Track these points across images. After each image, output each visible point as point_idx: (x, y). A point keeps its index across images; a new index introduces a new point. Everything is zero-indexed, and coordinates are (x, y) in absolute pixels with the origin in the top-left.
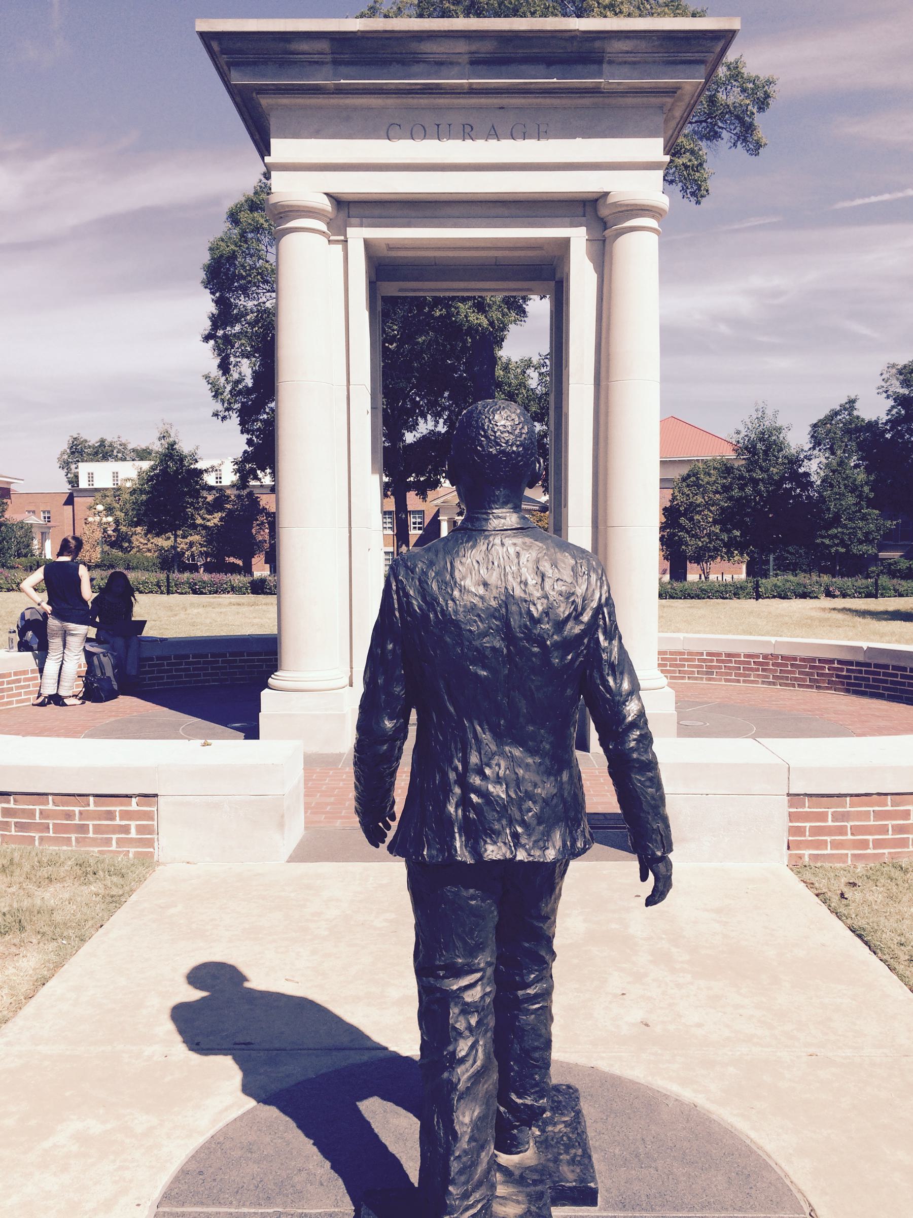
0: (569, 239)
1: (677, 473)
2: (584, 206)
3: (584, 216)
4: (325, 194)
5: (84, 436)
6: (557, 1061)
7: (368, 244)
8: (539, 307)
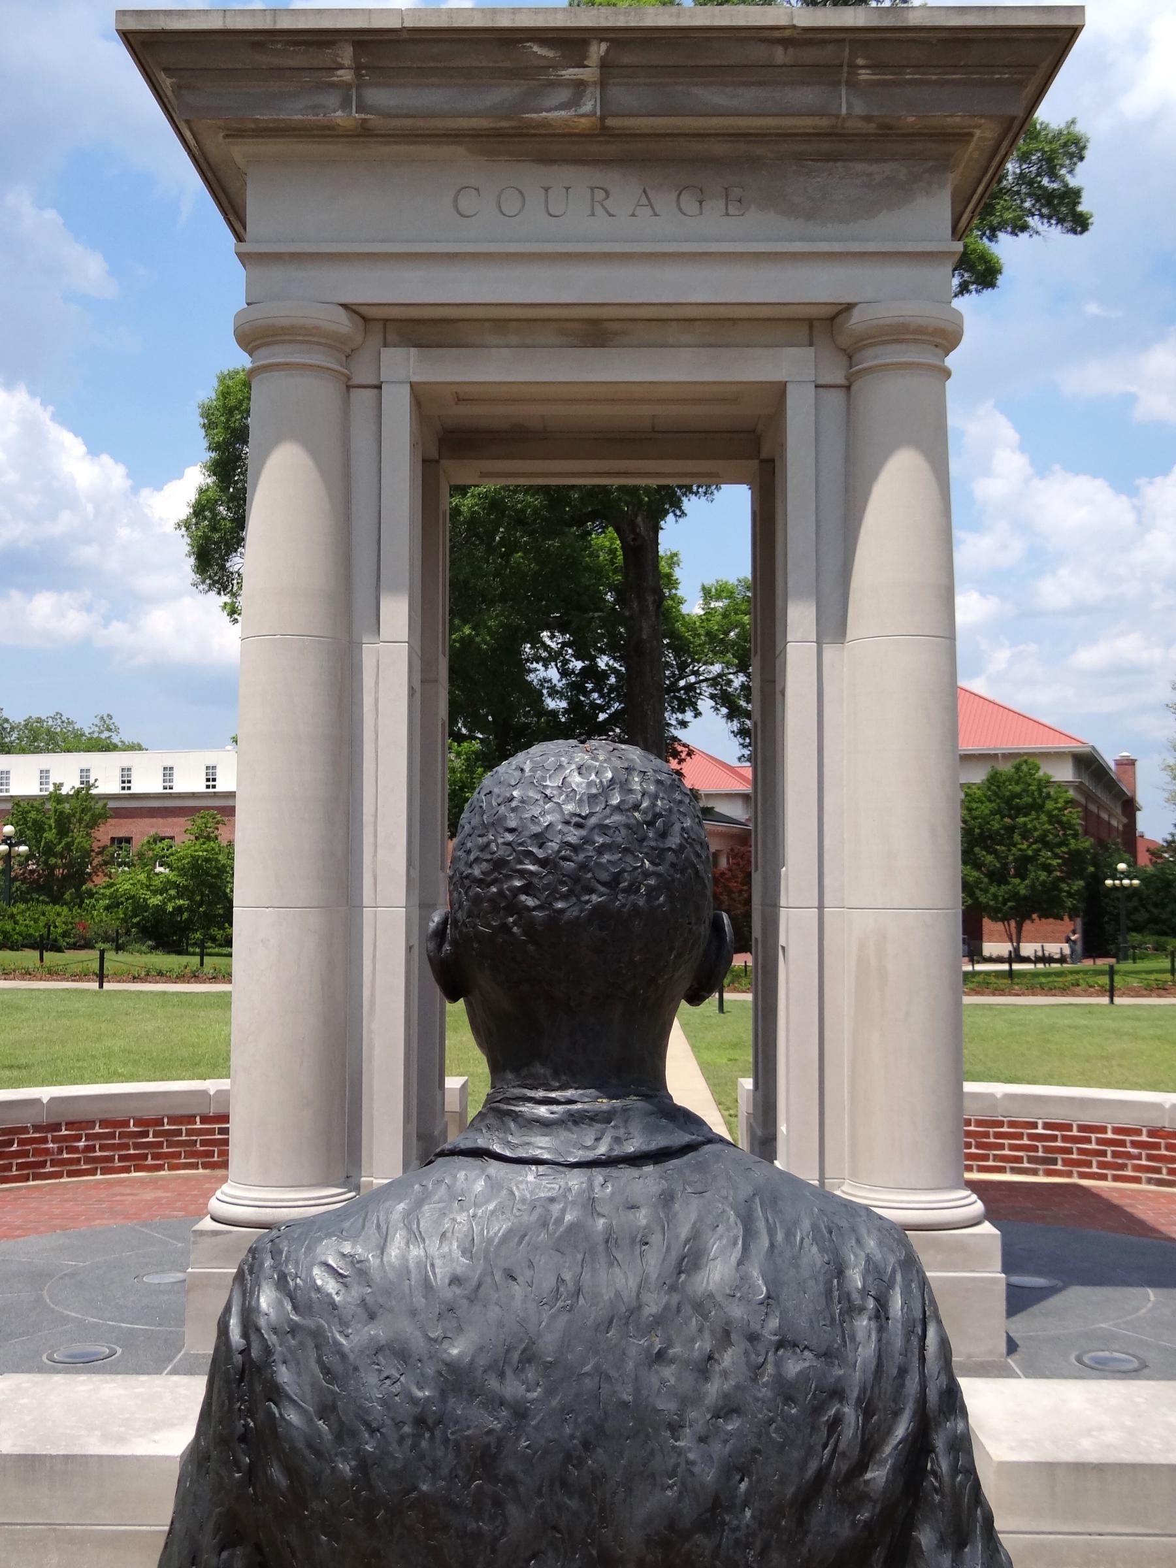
0: (784, 385)
1: (977, 776)
2: (811, 327)
3: (811, 345)
4: (341, 305)
5: (1085, 196)
6: (1008, 1469)
7: (420, 396)
8: (736, 499)
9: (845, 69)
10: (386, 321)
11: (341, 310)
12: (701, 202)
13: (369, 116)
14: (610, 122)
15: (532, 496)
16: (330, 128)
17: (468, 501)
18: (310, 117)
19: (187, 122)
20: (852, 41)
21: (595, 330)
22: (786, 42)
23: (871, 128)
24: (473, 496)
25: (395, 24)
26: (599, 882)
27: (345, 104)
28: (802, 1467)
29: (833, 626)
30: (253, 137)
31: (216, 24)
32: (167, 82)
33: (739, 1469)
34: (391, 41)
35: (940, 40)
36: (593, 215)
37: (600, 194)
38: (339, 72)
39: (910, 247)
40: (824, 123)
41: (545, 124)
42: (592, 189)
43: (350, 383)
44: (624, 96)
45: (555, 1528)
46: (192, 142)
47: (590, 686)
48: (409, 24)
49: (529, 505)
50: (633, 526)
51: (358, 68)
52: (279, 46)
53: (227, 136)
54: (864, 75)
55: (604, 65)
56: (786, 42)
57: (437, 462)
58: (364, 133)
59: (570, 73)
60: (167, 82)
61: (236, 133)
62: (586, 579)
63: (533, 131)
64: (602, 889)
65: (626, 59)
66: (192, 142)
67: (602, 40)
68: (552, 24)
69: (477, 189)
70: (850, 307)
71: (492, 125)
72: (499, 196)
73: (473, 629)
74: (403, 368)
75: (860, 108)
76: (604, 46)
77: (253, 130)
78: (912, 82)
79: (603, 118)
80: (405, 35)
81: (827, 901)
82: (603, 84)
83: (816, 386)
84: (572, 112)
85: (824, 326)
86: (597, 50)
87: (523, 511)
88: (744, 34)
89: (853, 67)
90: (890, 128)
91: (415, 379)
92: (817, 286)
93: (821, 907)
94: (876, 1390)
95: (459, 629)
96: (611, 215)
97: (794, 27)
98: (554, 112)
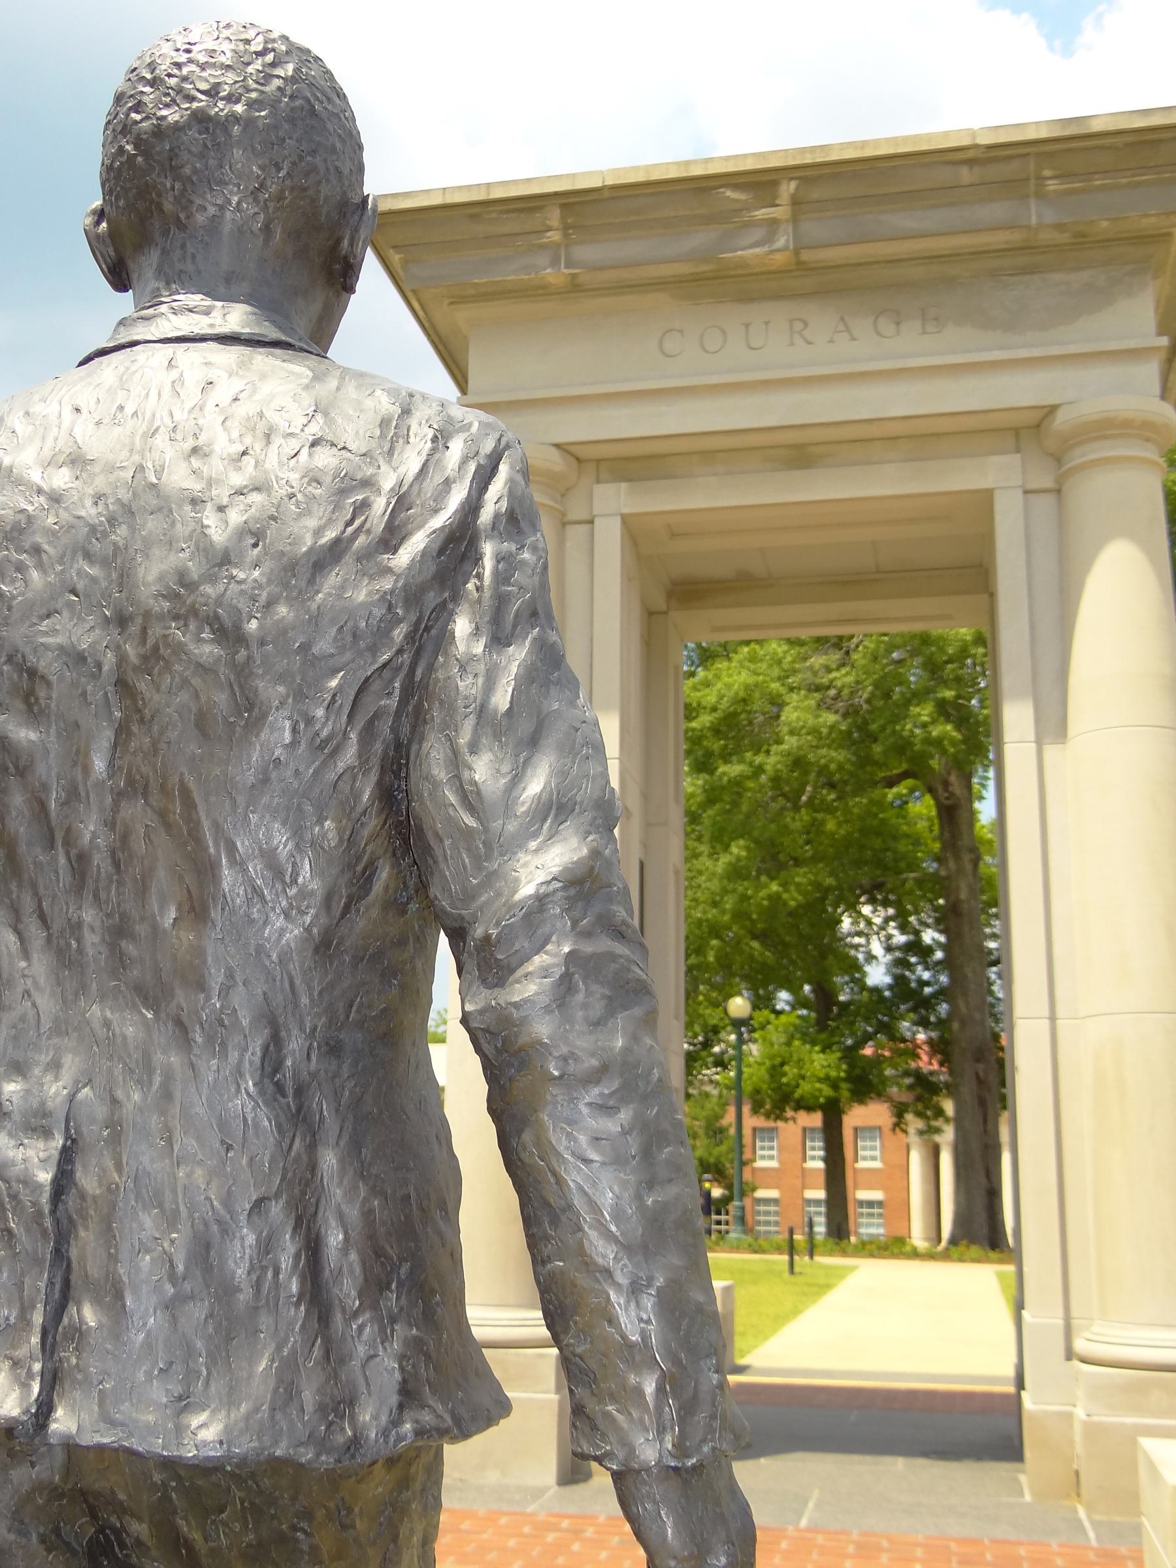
3: (1018, 451)
7: (634, 530)
9: (1032, 182)
10: (599, 461)
11: (554, 450)
12: (898, 324)
13: (576, 271)
14: (806, 256)
15: (836, 750)
16: (542, 287)
17: (772, 760)
18: (522, 277)
19: (414, 291)
20: (1038, 155)
21: (799, 452)
22: (971, 162)
23: (1064, 238)
24: (776, 754)
25: (596, 183)
26: (198, 90)
27: (555, 262)
28: (318, 532)
29: (1053, 725)
30: (473, 302)
31: (437, 200)
32: (395, 258)
33: (253, 534)
34: (595, 201)
35: (1127, 145)
36: (792, 344)
37: (798, 326)
38: (549, 234)
39: (1113, 345)
40: (1015, 237)
41: (742, 264)
42: (791, 321)
43: (565, 520)
44: (814, 229)
45: (74, 592)
46: (421, 313)
47: (913, 960)
48: (610, 182)
49: (832, 760)
50: (946, 784)
51: (566, 228)
52: (494, 215)
53: (451, 303)
54: (1052, 186)
55: (795, 202)
56: (971, 162)
57: (665, 613)
58: (575, 288)
59: (762, 213)
60: (395, 258)
61: (459, 300)
62: (903, 847)
63: (732, 273)
64: (203, 97)
65: (815, 195)
66: (421, 313)
67: (792, 179)
68: (742, 168)
69: (681, 331)
70: (1053, 409)
71: (693, 270)
72: (702, 336)
73: (780, 885)
74: (613, 502)
75: (1050, 217)
76: (793, 185)
77: (474, 296)
78: (1103, 188)
79: (796, 252)
80: (607, 194)
81: (1060, 1011)
82: (795, 220)
83: (1026, 492)
84: (766, 248)
85: (1029, 431)
86: (788, 189)
87: (826, 766)
88: (927, 159)
89: (1041, 179)
90: (1084, 235)
91: (626, 511)
92: (1019, 391)
93: (1053, 1018)
94: (416, 488)
95: (766, 886)
96: (809, 343)
97: (977, 146)
98: (749, 252)
